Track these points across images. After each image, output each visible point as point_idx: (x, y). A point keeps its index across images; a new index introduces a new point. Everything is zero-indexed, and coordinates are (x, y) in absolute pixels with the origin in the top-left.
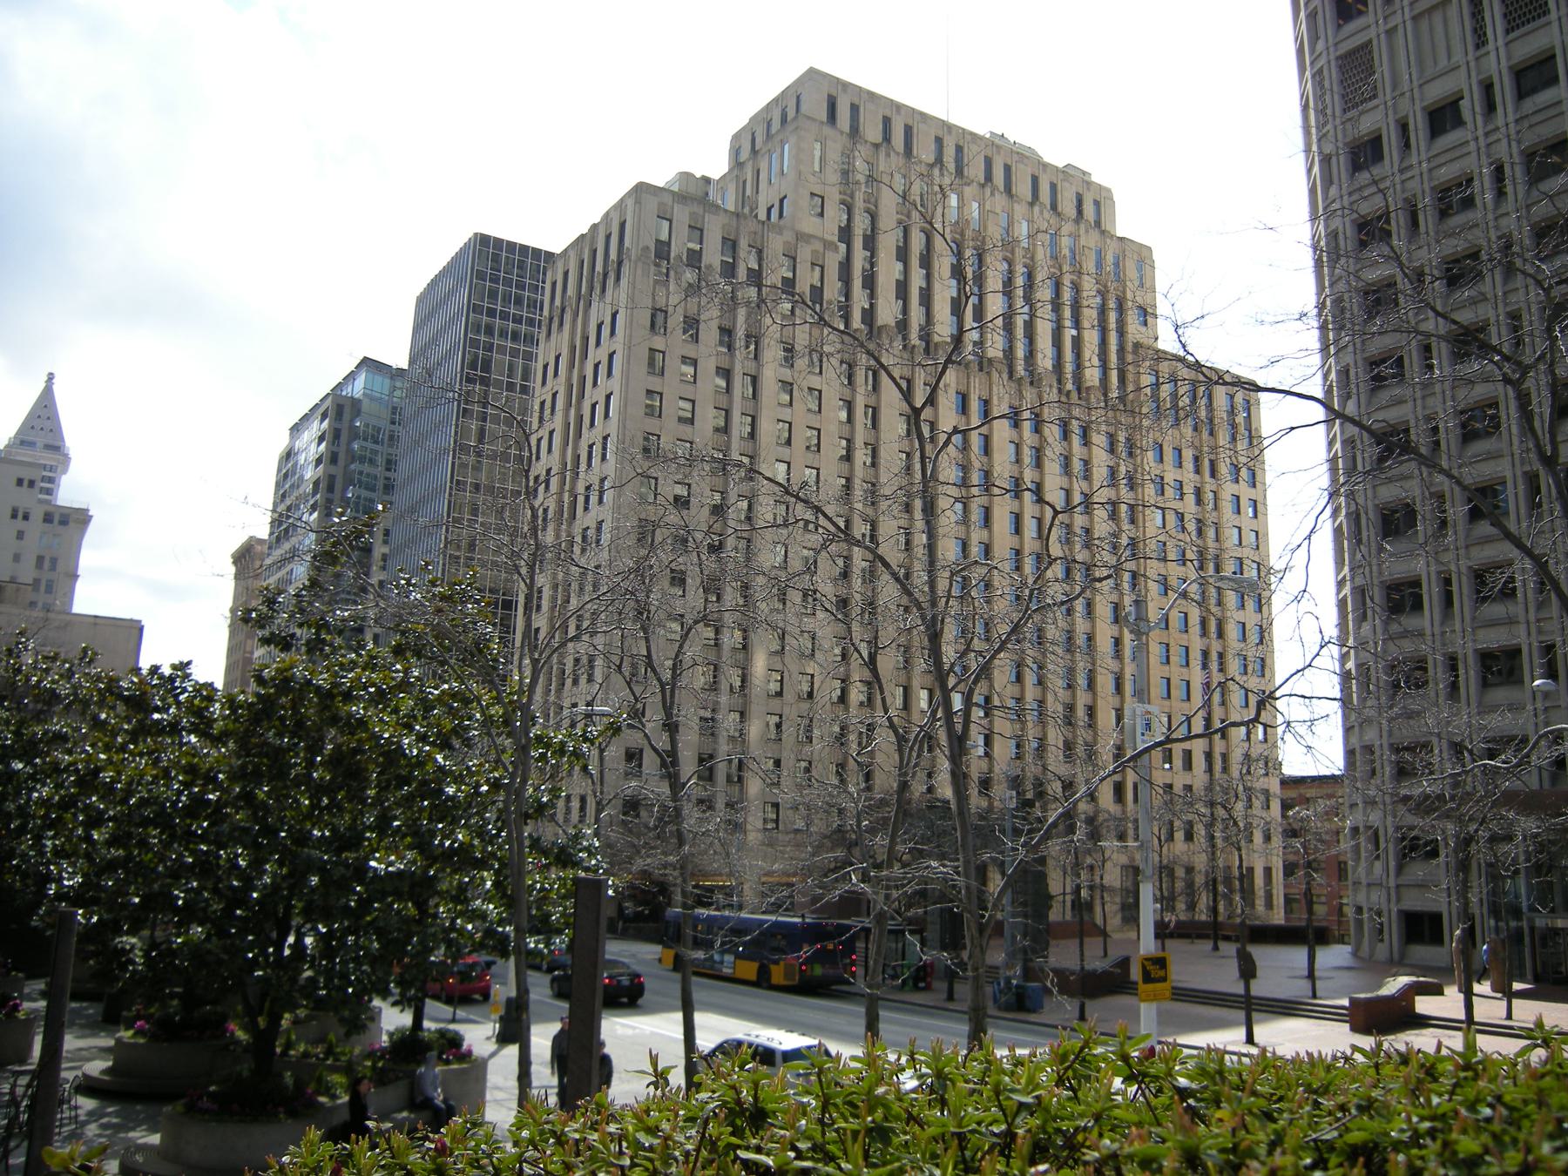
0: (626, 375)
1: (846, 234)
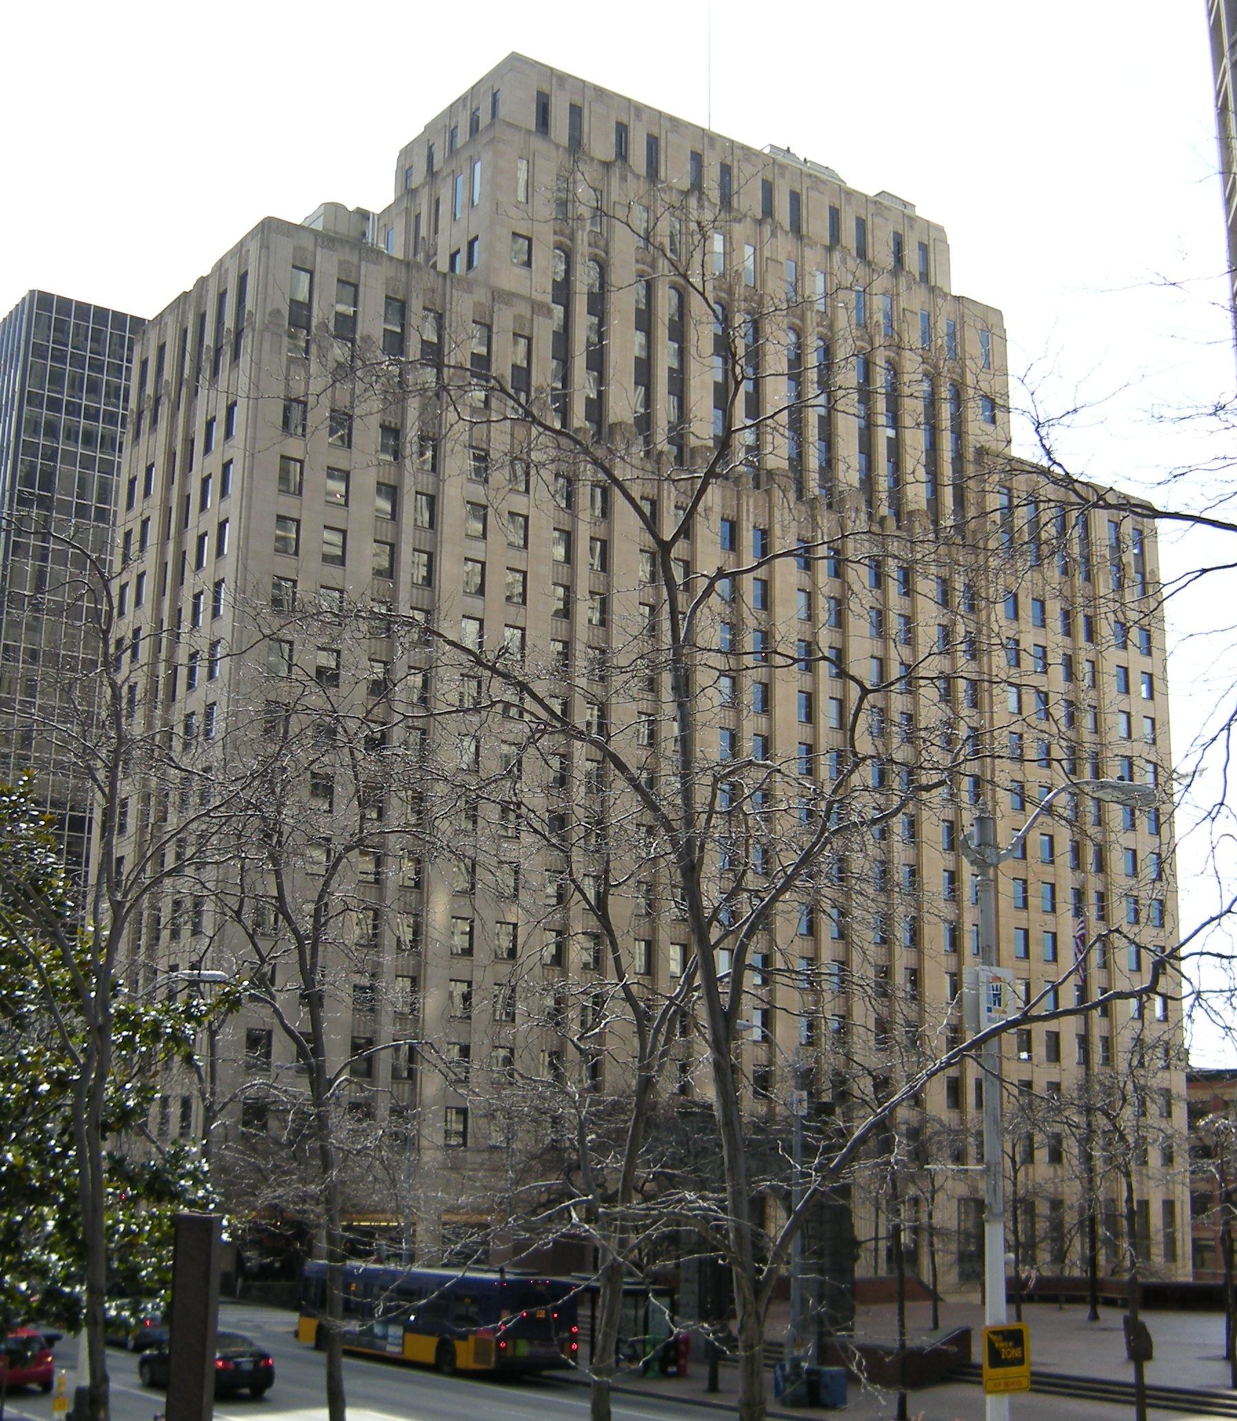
0: (248, 494)
1: (563, 292)
